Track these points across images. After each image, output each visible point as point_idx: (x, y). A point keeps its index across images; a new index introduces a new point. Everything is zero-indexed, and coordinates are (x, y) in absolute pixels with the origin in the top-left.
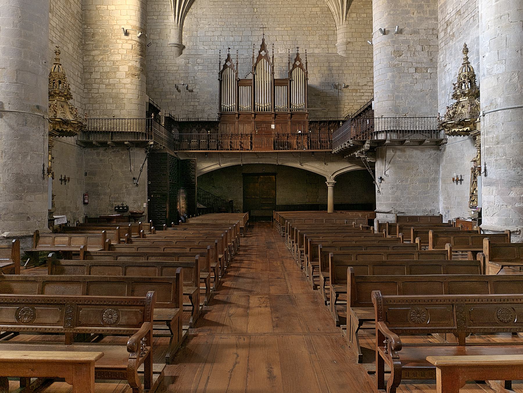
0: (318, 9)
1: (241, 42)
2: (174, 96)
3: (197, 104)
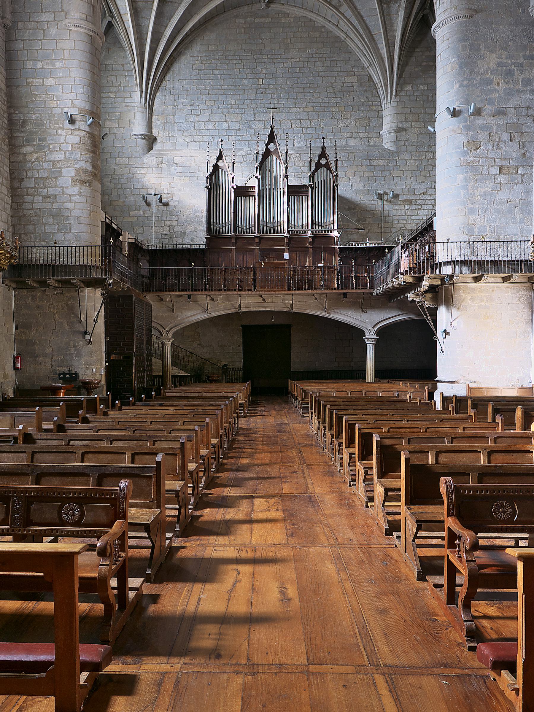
0: (354, 79)
1: (239, 130)
2: (141, 212)
3: (174, 223)
